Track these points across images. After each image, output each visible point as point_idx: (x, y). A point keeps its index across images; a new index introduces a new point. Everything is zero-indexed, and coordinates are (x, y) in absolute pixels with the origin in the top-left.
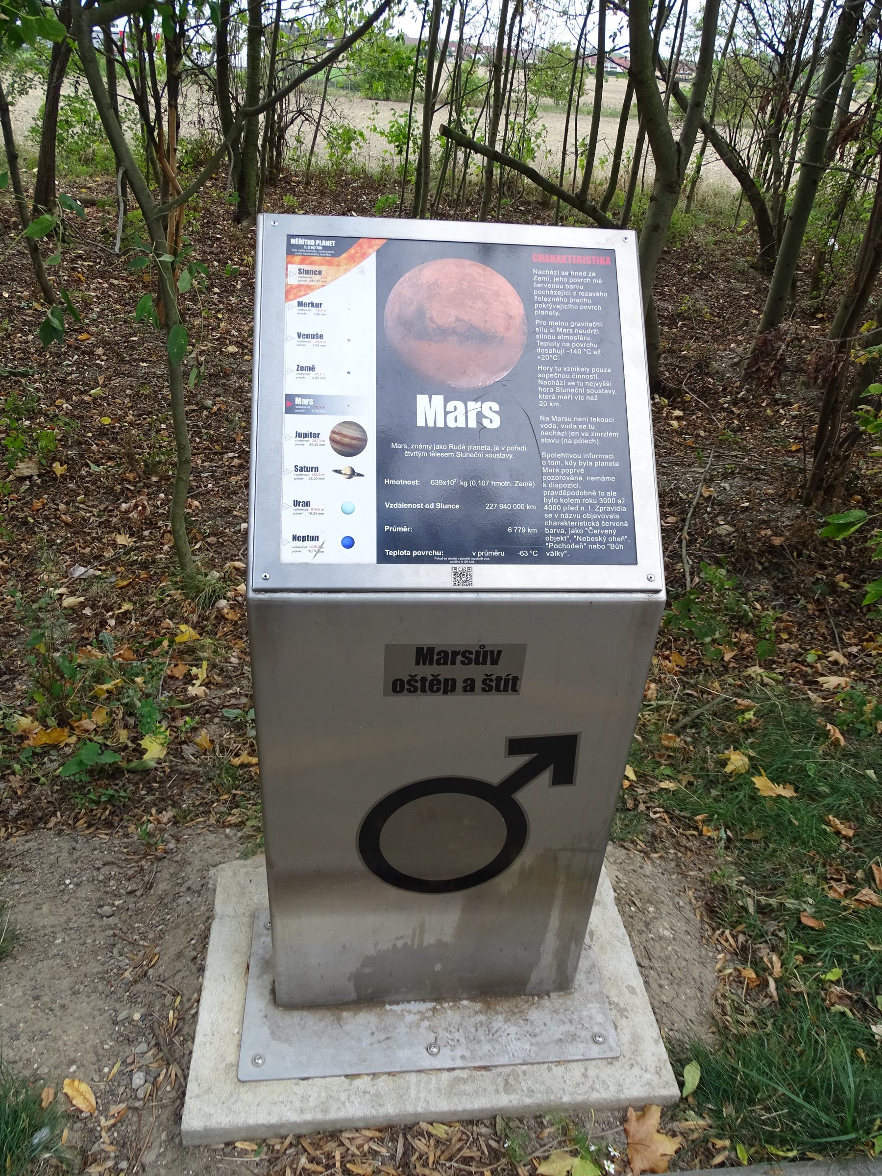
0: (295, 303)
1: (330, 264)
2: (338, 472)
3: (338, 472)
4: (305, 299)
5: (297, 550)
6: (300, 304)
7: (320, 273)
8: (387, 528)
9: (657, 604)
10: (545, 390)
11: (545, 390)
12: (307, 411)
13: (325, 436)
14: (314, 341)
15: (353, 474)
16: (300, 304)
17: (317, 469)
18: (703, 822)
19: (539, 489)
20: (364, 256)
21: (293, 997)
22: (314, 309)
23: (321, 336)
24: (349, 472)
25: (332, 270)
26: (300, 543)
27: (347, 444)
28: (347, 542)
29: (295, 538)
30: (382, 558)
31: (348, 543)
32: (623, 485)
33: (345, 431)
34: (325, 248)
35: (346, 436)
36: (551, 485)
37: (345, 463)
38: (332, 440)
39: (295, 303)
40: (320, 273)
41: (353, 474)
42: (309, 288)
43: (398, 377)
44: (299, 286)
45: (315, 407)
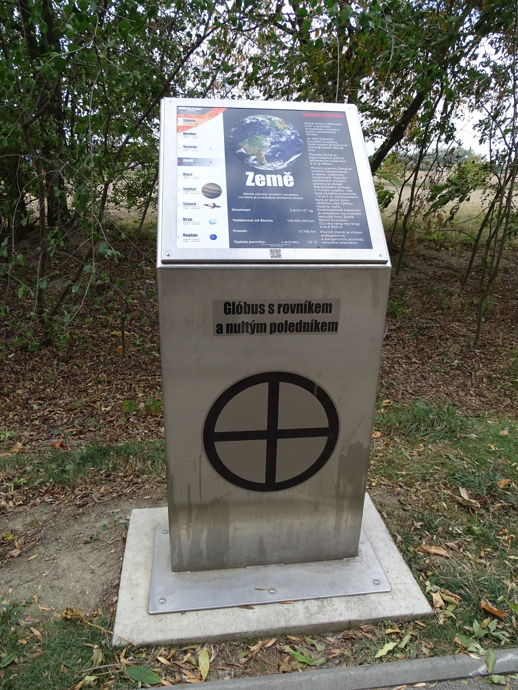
0: (182, 133)
1: (199, 117)
2: (207, 205)
3: (207, 205)
4: (186, 132)
5: (186, 241)
6: (184, 134)
7: (194, 121)
8: (234, 231)
9: (387, 268)
10: (316, 181)
11: (316, 181)
12: (189, 164)
13: (199, 189)
14: (192, 149)
15: (215, 206)
16: (184, 134)
17: (195, 204)
18: (509, 627)
19: (315, 212)
20: (217, 114)
21: (186, 563)
22: (192, 136)
23: (196, 147)
24: (212, 205)
25: (200, 120)
26: (188, 238)
27: (212, 192)
28: (213, 237)
29: (184, 235)
30: (232, 245)
31: (214, 237)
32: (359, 202)
33: (209, 187)
34: (196, 111)
35: (210, 190)
36: (323, 213)
37: (211, 201)
38: (203, 191)
39: (182, 133)
40: (194, 121)
41: (215, 206)
42: (189, 127)
43: (236, 160)
44: (183, 126)
45: (193, 163)
